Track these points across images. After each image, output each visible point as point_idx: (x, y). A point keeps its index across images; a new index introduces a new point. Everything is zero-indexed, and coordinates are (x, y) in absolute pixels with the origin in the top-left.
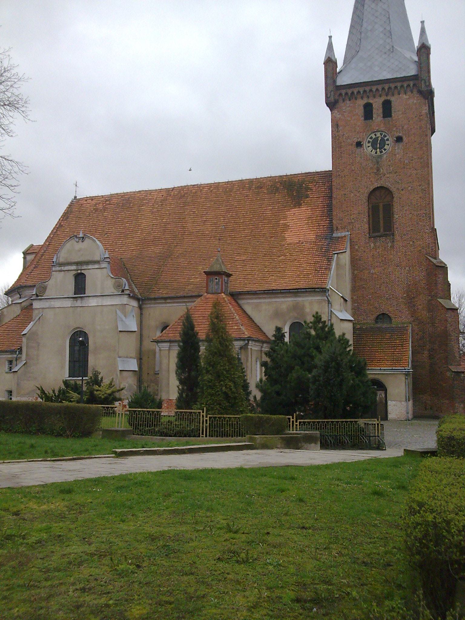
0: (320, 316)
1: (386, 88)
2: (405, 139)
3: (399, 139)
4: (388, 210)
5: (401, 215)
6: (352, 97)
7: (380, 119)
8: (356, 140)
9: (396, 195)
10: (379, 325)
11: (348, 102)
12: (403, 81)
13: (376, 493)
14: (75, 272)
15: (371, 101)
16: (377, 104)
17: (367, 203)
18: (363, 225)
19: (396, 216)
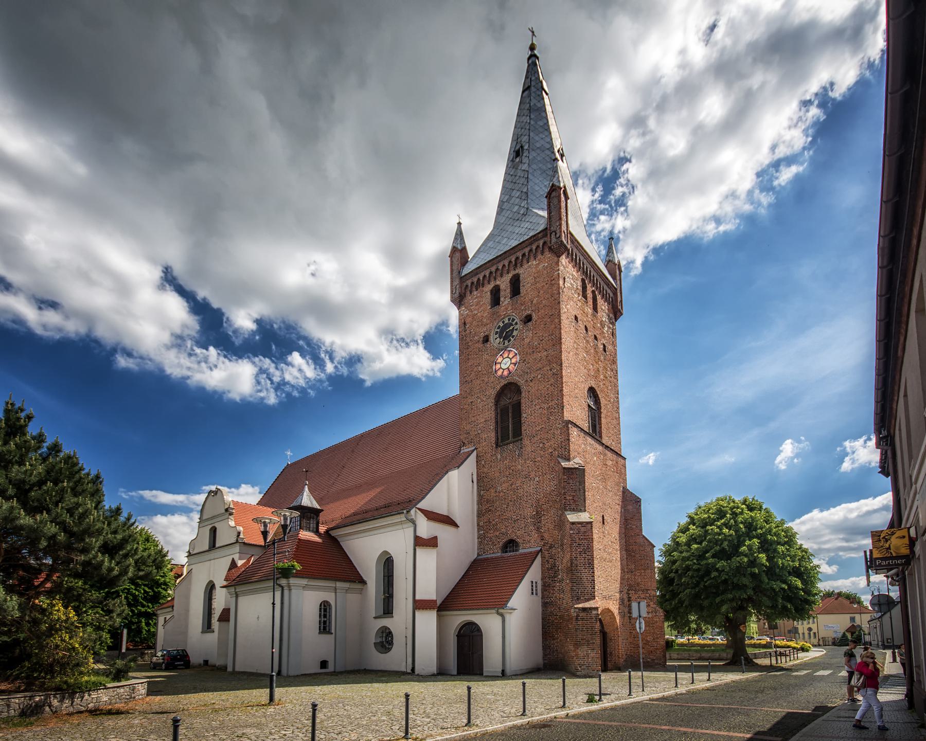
0: (877, 448)
1: (513, 260)
2: (534, 317)
3: (528, 319)
4: (517, 408)
5: (531, 415)
6: (479, 285)
7: (508, 300)
8: (482, 335)
9: (524, 388)
10: (333, 631)
11: (475, 293)
12: (531, 244)
13: (605, 350)
14: (333, 604)
15: (498, 283)
16: (504, 283)
17: (493, 408)
18: (490, 436)
19: (524, 415)
